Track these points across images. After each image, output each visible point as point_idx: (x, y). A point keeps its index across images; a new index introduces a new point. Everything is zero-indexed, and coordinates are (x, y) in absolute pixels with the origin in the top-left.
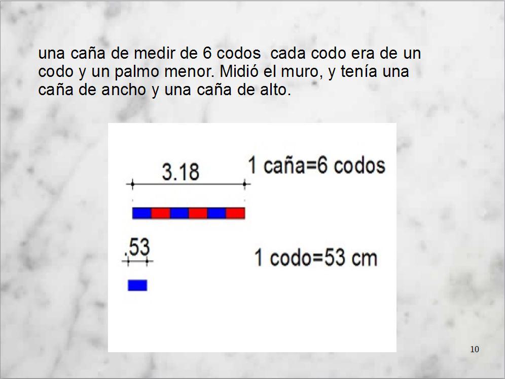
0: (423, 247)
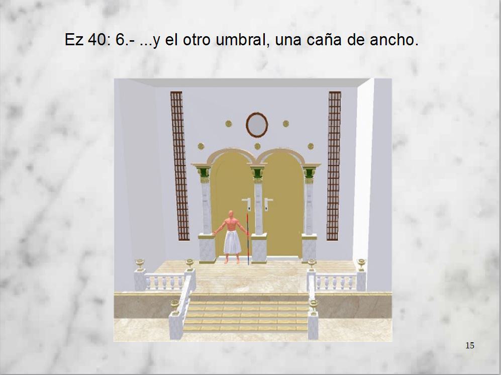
0: (419, 243)
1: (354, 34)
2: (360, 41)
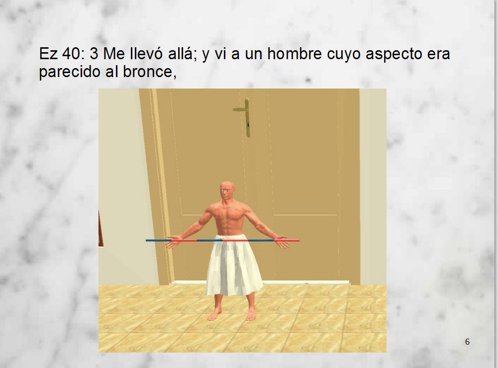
0: (415, 241)
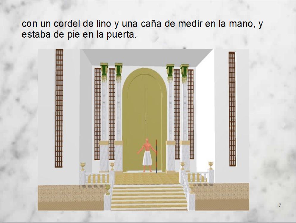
1: (169, 20)
2: (172, 24)
